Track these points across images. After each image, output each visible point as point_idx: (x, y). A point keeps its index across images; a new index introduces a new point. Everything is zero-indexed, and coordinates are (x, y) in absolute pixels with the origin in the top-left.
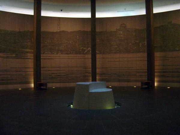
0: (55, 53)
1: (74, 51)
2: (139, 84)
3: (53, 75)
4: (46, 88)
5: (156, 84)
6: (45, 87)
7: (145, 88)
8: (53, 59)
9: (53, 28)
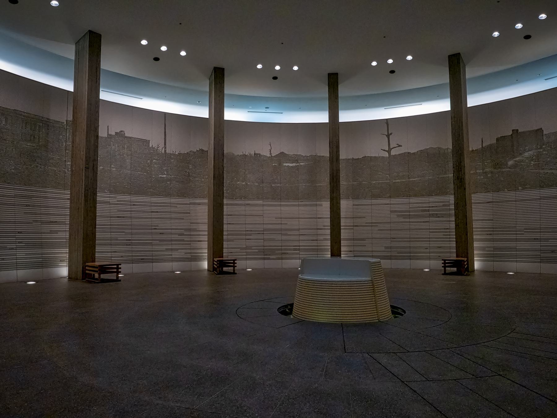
2: (438, 264)
4: (234, 270)
5: (477, 265)
9: (375, 148)
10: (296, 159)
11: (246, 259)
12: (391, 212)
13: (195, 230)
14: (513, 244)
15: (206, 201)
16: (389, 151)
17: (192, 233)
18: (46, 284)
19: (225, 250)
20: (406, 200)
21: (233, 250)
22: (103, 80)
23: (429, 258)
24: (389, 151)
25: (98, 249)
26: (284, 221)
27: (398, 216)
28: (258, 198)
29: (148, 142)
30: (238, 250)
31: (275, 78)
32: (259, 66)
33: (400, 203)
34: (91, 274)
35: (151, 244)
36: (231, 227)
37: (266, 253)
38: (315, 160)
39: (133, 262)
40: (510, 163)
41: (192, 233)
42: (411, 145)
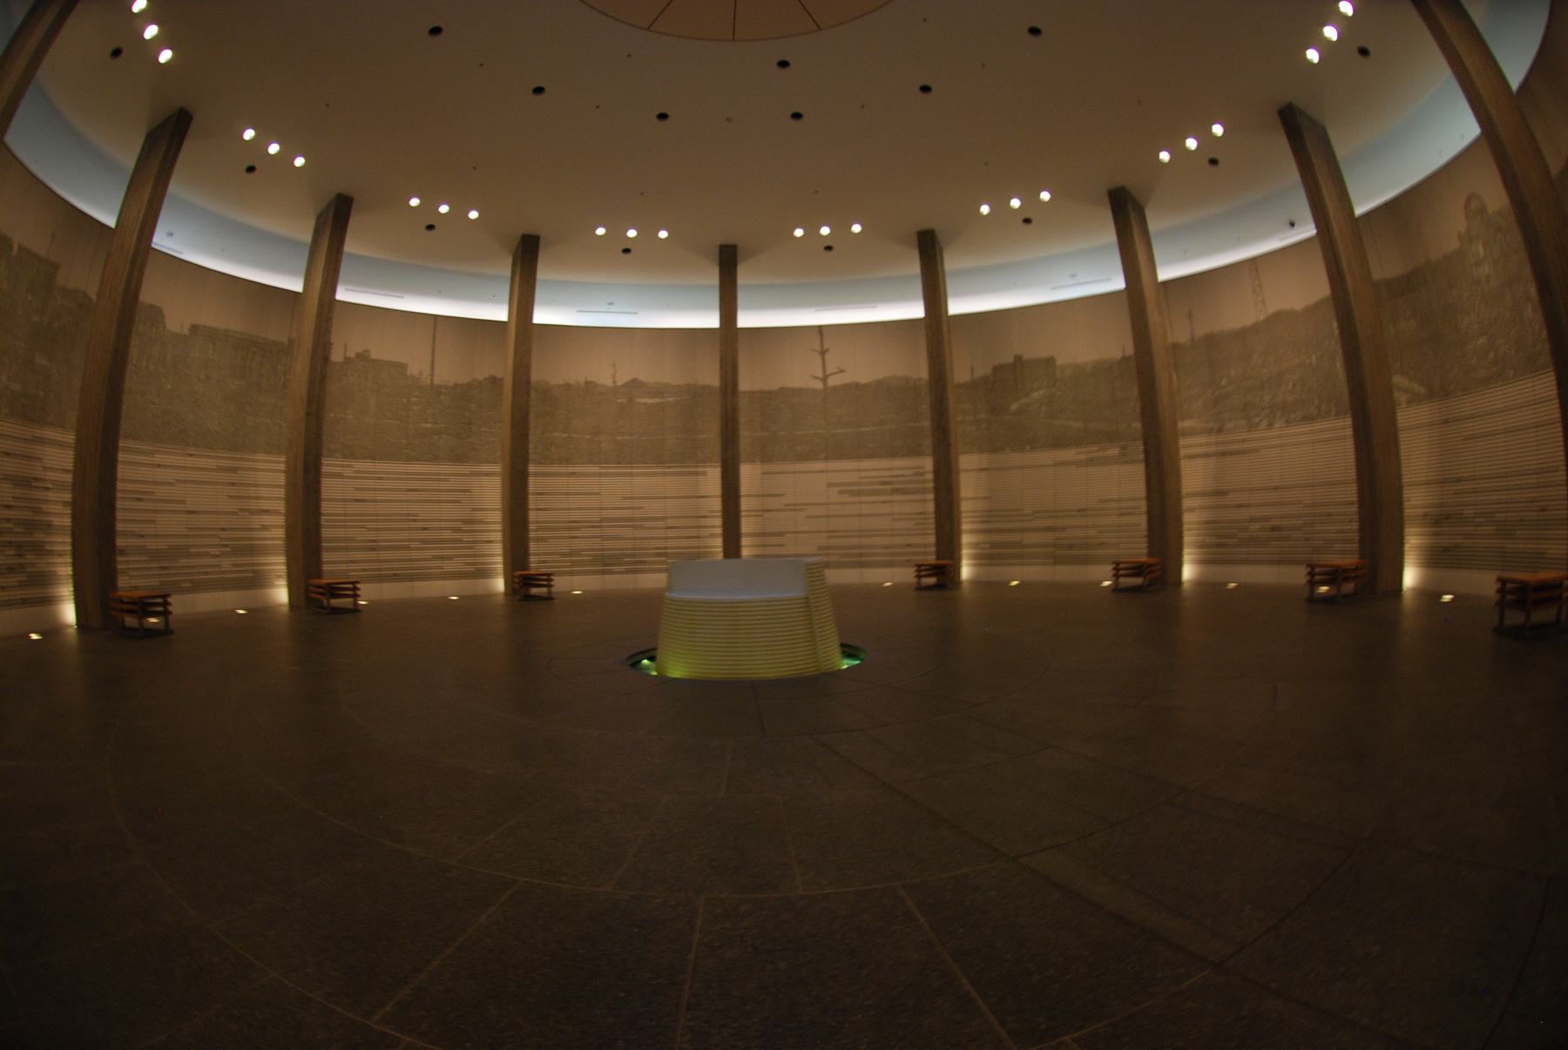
0: (1264, 424)
1: (41, 360)
3: (1256, 526)
5: (1188, 572)
6: (544, 590)
7: (1326, 599)
8: (1257, 450)
9: (800, 374)
10: (658, 390)
11: (571, 573)
12: (830, 485)
13: (480, 522)
14: (1016, 537)
15: (497, 468)
16: (824, 379)
17: (477, 527)
18: (261, 613)
19: (532, 559)
20: (852, 464)
21: (550, 558)
22: (345, 268)
23: (891, 564)
24: (824, 379)
25: (326, 556)
26: (637, 503)
27: (841, 492)
28: (591, 462)
29: (403, 366)
30: (556, 558)
31: (627, 251)
32: (601, 231)
33: (848, 470)
34: (321, 598)
35: (408, 548)
36: (543, 516)
37: (605, 562)
38: (695, 393)
39: (380, 579)
40: (1014, 407)
41: (477, 527)
42: (860, 369)
